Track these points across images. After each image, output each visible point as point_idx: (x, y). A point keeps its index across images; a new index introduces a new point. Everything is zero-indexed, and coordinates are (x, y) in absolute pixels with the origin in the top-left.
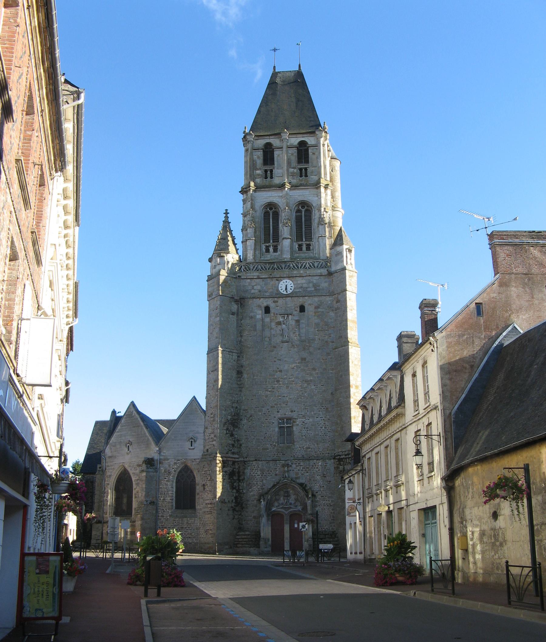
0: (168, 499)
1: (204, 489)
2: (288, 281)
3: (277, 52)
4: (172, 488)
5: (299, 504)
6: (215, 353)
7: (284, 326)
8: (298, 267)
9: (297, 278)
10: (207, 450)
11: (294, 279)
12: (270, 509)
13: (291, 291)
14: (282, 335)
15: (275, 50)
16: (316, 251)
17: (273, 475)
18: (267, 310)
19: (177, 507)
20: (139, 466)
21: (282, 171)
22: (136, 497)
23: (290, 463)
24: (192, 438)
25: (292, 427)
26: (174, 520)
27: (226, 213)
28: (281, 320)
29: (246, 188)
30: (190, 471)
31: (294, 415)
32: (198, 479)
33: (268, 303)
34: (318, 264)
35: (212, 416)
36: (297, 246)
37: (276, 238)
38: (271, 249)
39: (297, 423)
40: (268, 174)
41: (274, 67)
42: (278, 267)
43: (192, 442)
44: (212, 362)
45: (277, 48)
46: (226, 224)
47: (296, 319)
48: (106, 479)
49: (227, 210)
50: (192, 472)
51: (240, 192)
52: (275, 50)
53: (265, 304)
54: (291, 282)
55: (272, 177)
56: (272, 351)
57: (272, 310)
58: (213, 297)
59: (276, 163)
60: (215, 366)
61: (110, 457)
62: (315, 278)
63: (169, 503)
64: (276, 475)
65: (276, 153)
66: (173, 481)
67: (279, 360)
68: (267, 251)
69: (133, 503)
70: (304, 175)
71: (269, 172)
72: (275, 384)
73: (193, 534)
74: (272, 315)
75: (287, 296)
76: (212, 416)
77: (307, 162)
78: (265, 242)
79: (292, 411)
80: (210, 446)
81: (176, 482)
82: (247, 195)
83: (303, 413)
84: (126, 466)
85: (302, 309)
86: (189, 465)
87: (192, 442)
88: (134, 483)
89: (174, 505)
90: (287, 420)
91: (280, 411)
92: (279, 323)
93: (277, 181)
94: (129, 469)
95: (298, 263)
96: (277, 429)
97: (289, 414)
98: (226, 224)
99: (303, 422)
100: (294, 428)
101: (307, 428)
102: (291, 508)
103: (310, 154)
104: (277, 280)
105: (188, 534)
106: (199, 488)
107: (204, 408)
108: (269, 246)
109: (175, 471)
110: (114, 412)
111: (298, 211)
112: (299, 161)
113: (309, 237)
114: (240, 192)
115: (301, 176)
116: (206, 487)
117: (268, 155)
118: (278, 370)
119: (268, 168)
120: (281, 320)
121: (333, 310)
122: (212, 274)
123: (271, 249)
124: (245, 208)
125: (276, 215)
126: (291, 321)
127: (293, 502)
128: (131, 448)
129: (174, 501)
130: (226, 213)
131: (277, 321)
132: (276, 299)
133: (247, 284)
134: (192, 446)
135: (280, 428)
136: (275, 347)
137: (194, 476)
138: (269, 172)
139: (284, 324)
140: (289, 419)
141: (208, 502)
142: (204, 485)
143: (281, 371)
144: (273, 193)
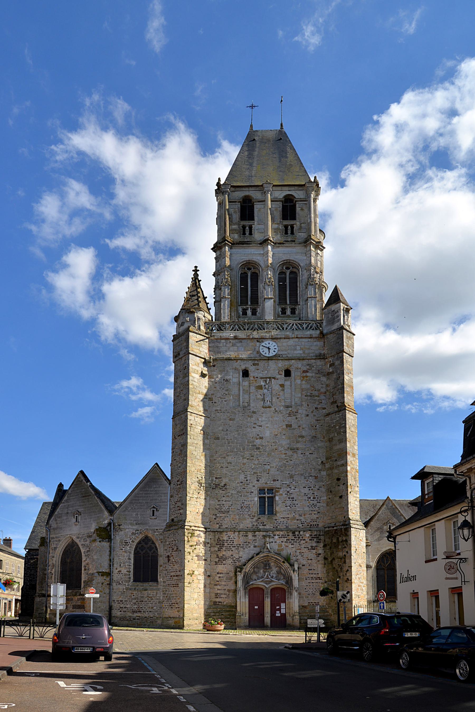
0: (124, 571)
1: (169, 560)
2: (271, 343)
3: (255, 109)
4: (130, 559)
5: (282, 578)
6: (182, 416)
7: (266, 391)
8: (283, 329)
9: (282, 340)
10: (173, 520)
11: (279, 340)
12: (248, 583)
13: (274, 354)
14: (264, 400)
15: (252, 107)
16: (304, 314)
17: (252, 547)
18: (246, 374)
19: (135, 581)
20: (90, 537)
21: (268, 223)
22: (85, 570)
23: (272, 535)
24: (154, 507)
25: (275, 496)
26: (132, 594)
27: (196, 270)
28: (263, 384)
29: (220, 243)
30: (151, 542)
31: (277, 484)
32: (161, 551)
33: (247, 366)
34: (308, 326)
35: (179, 483)
36: (280, 310)
37: (255, 300)
38: (249, 312)
39: (281, 492)
40: (247, 231)
41: (251, 126)
42: (259, 327)
43: (153, 511)
44: (178, 426)
45: (254, 104)
46: (196, 281)
47: (280, 383)
48: (51, 552)
49: (196, 267)
50: (153, 543)
51: (212, 249)
52: (252, 107)
53: (243, 367)
54: (274, 344)
55: (251, 234)
56: (251, 417)
57: (251, 374)
58: (180, 357)
59: (256, 218)
60: (182, 430)
61: (54, 529)
62: (304, 340)
63: (125, 575)
64: (255, 547)
65: (257, 207)
66: (130, 553)
67: (259, 426)
68: (245, 313)
69: (83, 575)
70: (289, 232)
71: (247, 228)
72: (255, 451)
73: (155, 608)
74: (252, 378)
75: (269, 359)
76: (179, 483)
77: (293, 217)
78: (242, 304)
79: (274, 480)
80: (176, 516)
81: (135, 554)
82: (221, 252)
83: (288, 483)
84: (74, 538)
85: (288, 373)
86: (150, 535)
87: (153, 511)
88: (83, 554)
89: (132, 578)
90: (268, 490)
91: (260, 480)
92: (260, 387)
93: (257, 236)
94: (77, 541)
95: (283, 324)
96: (256, 499)
97: (271, 484)
98: (196, 281)
99: (289, 492)
100: (277, 498)
101: (293, 498)
102: (272, 581)
103: (298, 209)
104: (258, 341)
105: (149, 608)
106: (161, 561)
107: (170, 478)
108: (247, 309)
109: (133, 542)
110: (61, 485)
111: (281, 273)
112: (284, 217)
113: (295, 301)
114: (212, 249)
115: (286, 233)
116: (171, 558)
117: (247, 210)
118: (258, 437)
119: (247, 223)
120: (263, 384)
121: (324, 376)
122: (179, 333)
123: (249, 312)
124: (218, 266)
125: (255, 277)
126: (275, 385)
127: (274, 576)
128: (79, 518)
129: (132, 573)
130: (196, 270)
131: (257, 385)
132: (256, 362)
133: (221, 345)
134: (153, 515)
135: (260, 498)
136: (254, 412)
137: (156, 547)
138: (247, 228)
139: (266, 388)
140: (271, 490)
141: (172, 574)
142: (168, 556)
143: (261, 438)
144: (252, 250)
